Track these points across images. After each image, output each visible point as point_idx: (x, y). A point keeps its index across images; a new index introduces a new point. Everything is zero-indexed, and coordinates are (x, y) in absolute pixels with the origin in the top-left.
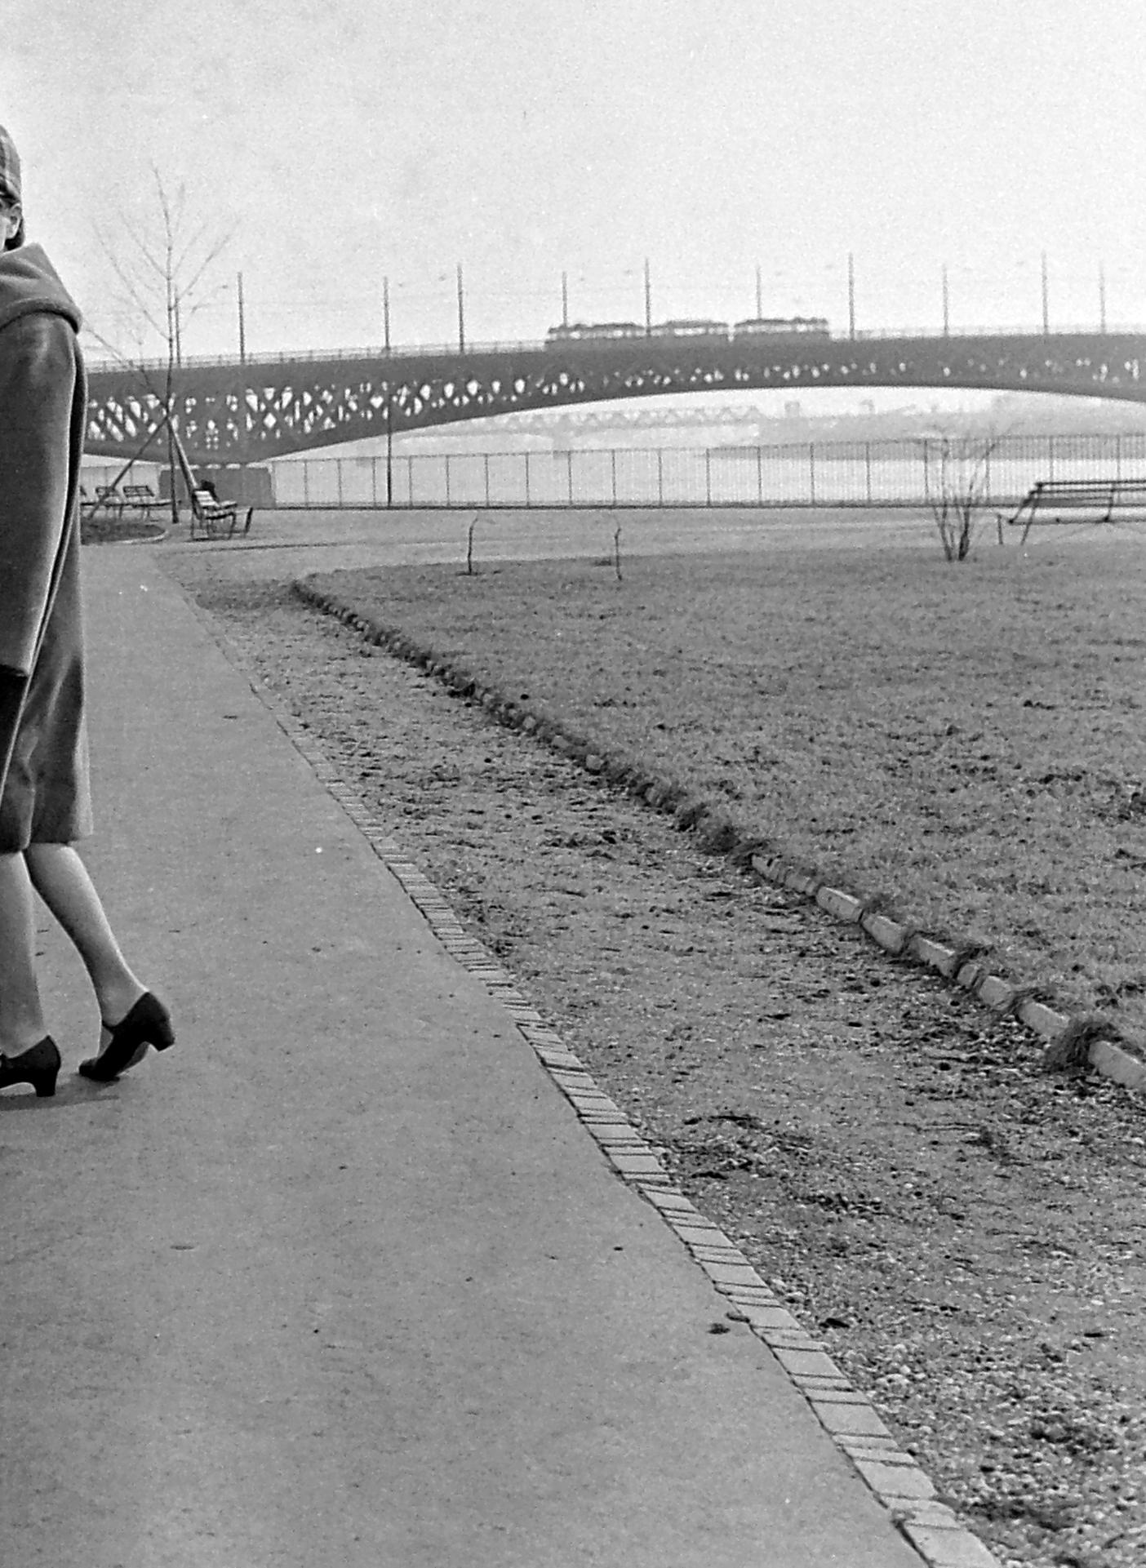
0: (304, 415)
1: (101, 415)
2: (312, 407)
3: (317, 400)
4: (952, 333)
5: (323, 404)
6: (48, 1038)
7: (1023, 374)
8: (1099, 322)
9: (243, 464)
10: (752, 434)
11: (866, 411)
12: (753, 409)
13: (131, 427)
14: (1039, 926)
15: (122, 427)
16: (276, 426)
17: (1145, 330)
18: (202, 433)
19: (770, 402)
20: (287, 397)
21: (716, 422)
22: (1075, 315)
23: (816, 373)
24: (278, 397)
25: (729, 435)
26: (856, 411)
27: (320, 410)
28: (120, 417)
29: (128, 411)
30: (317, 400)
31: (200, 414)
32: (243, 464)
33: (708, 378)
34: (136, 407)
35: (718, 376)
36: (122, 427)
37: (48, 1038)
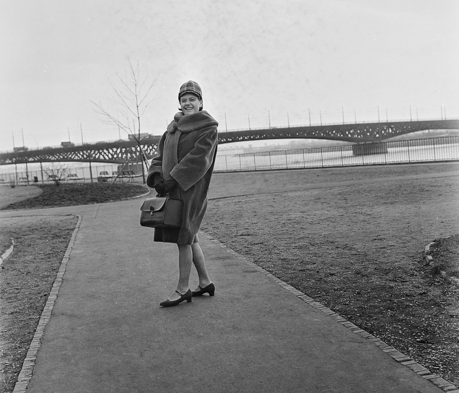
0: (150, 151)
1: (103, 154)
2: (152, 149)
3: (153, 148)
4: (290, 127)
5: (154, 149)
6: (155, 240)
7: (322, 134)
8: (343, 122)
9: (365, 142)
10: (241, 152)
11: (265, 146)
12: (242, 146)
13: (110, 156)
14: (206, 234)
15: (108, 156)
16: (117, 157)
17: (458, 119)
18: (126, 157)
19: (246, 144)
20: (146, 147)
21: (234, 149)
22: (316, 122)
23: (246, 138)
24: (144, 147)
25: (236, 152)
26: (263, 146)
27: (154, 150)
28: (107, 154)
29: (109, 152)
30: (153, 148)
31: (126, 152)
32: (365, 142)
33: (222, 141)
34: (111, 151)
35: (225, 140)
36: (108, 156)
37: (155, 240)
